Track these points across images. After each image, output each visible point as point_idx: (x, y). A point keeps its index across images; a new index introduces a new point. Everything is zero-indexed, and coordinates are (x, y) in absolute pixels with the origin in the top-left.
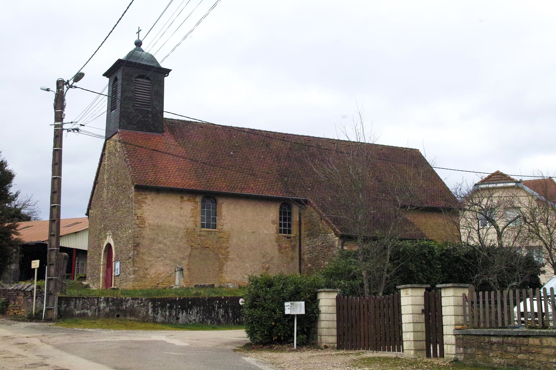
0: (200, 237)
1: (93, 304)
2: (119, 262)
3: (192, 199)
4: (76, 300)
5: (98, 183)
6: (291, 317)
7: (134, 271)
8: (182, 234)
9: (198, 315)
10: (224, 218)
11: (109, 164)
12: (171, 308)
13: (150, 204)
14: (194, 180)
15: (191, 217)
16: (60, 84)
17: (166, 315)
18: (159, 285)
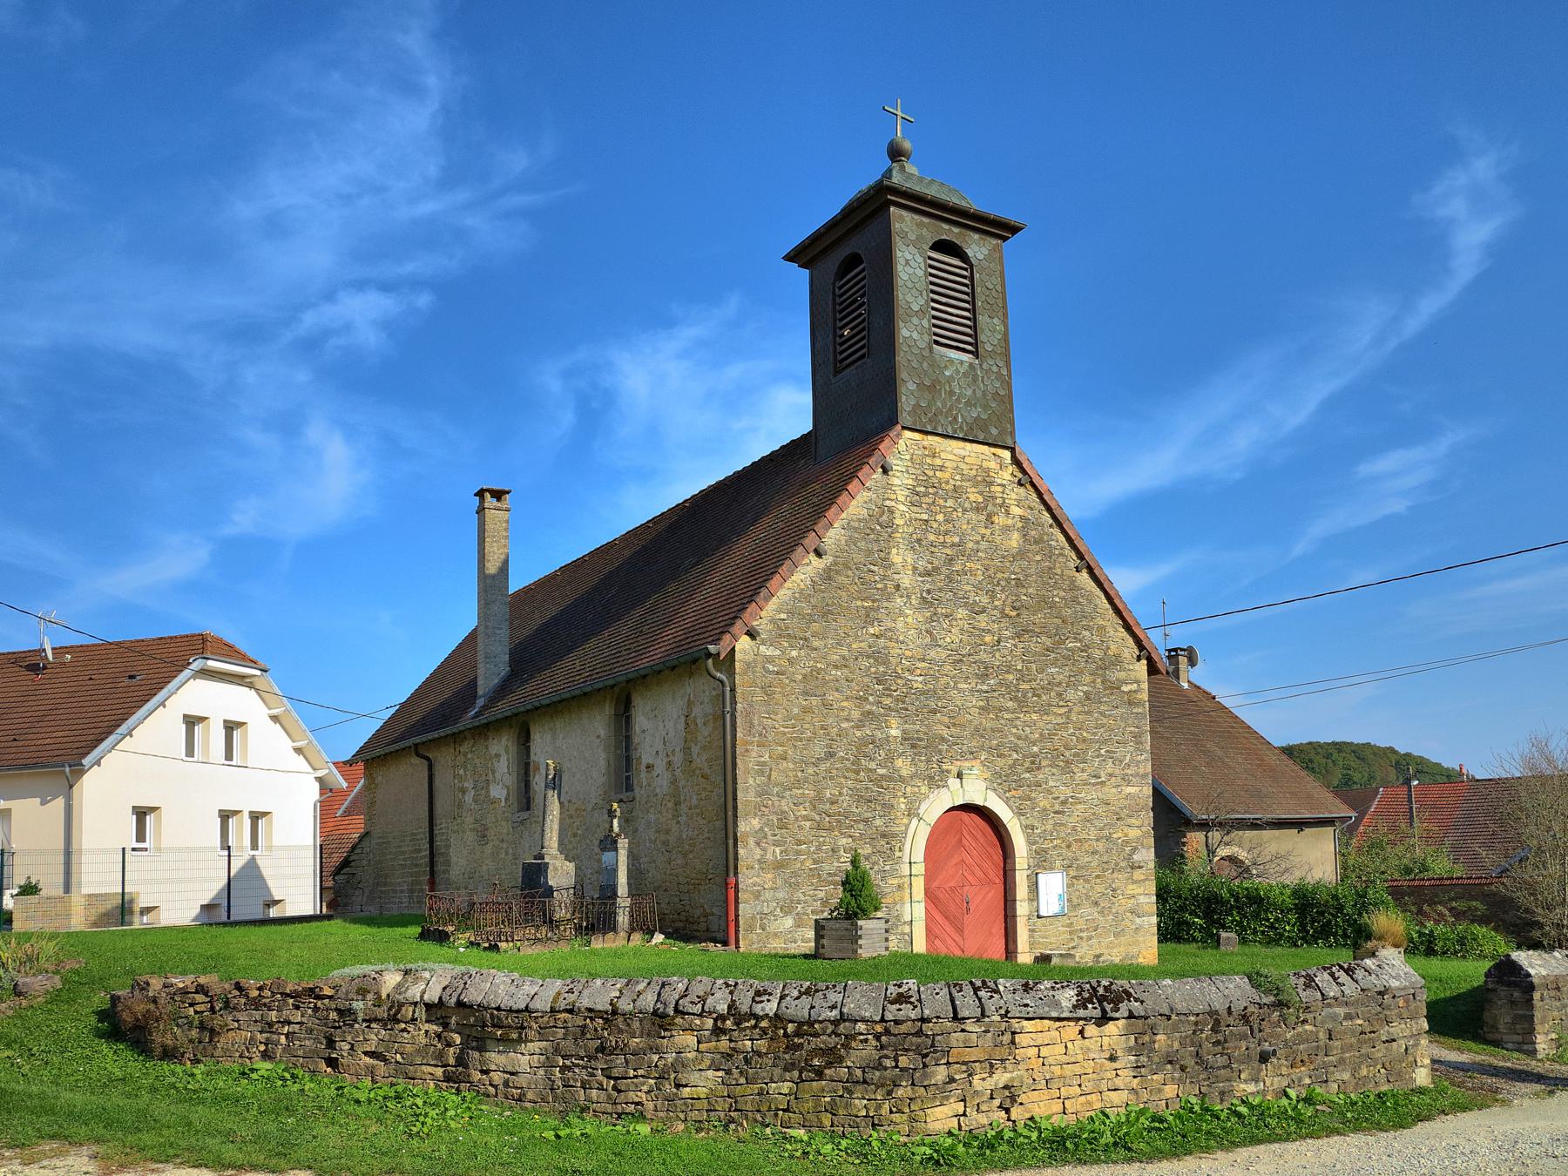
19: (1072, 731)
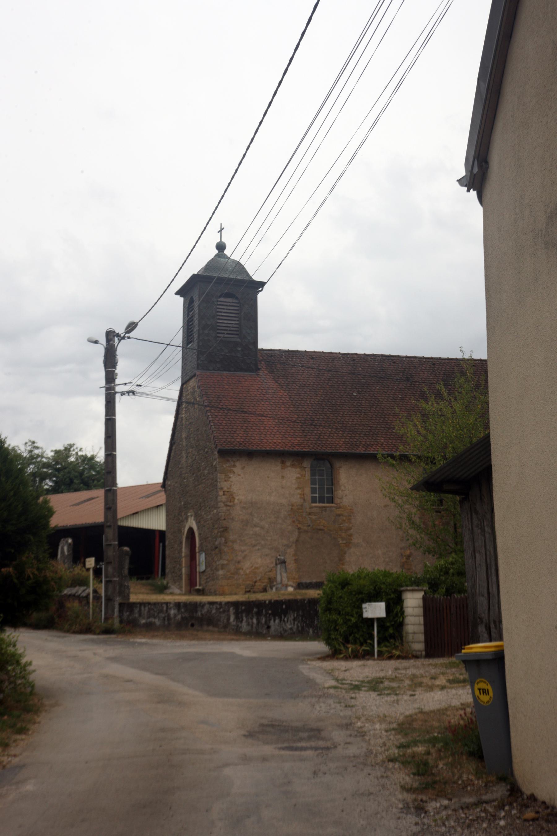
1: (161, 611)
3: (297, 464)
4: (140, 606)
5: (174, 443)
6: (371, 621)
8: (286, 513)
9: (296, 623)
10: (342, 488)
11: (188, 418)
12: (259, 614)
14: (300, 437)
15: (296, 489)
16: (110, 335)
17: (253, 623)
18: (256, 584)
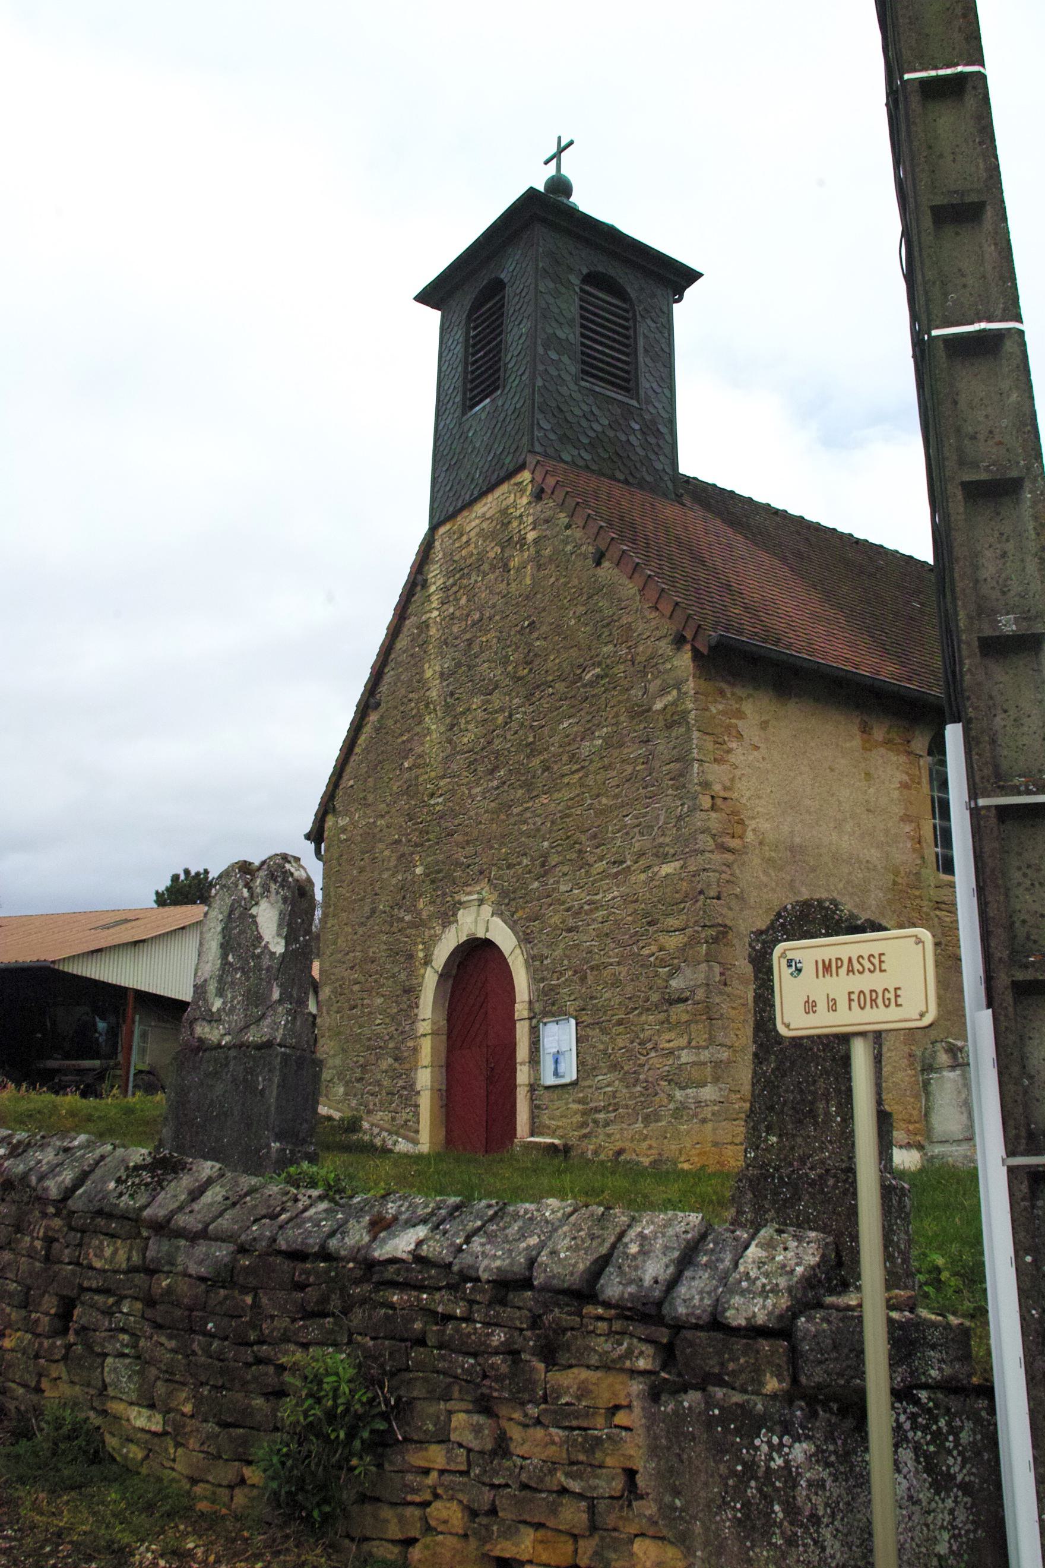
0: (938, 912)
2: (573, 1022)
7: (717, 1064)
13: (756, 740)
15: (902, 819)
19: (589, 802)
